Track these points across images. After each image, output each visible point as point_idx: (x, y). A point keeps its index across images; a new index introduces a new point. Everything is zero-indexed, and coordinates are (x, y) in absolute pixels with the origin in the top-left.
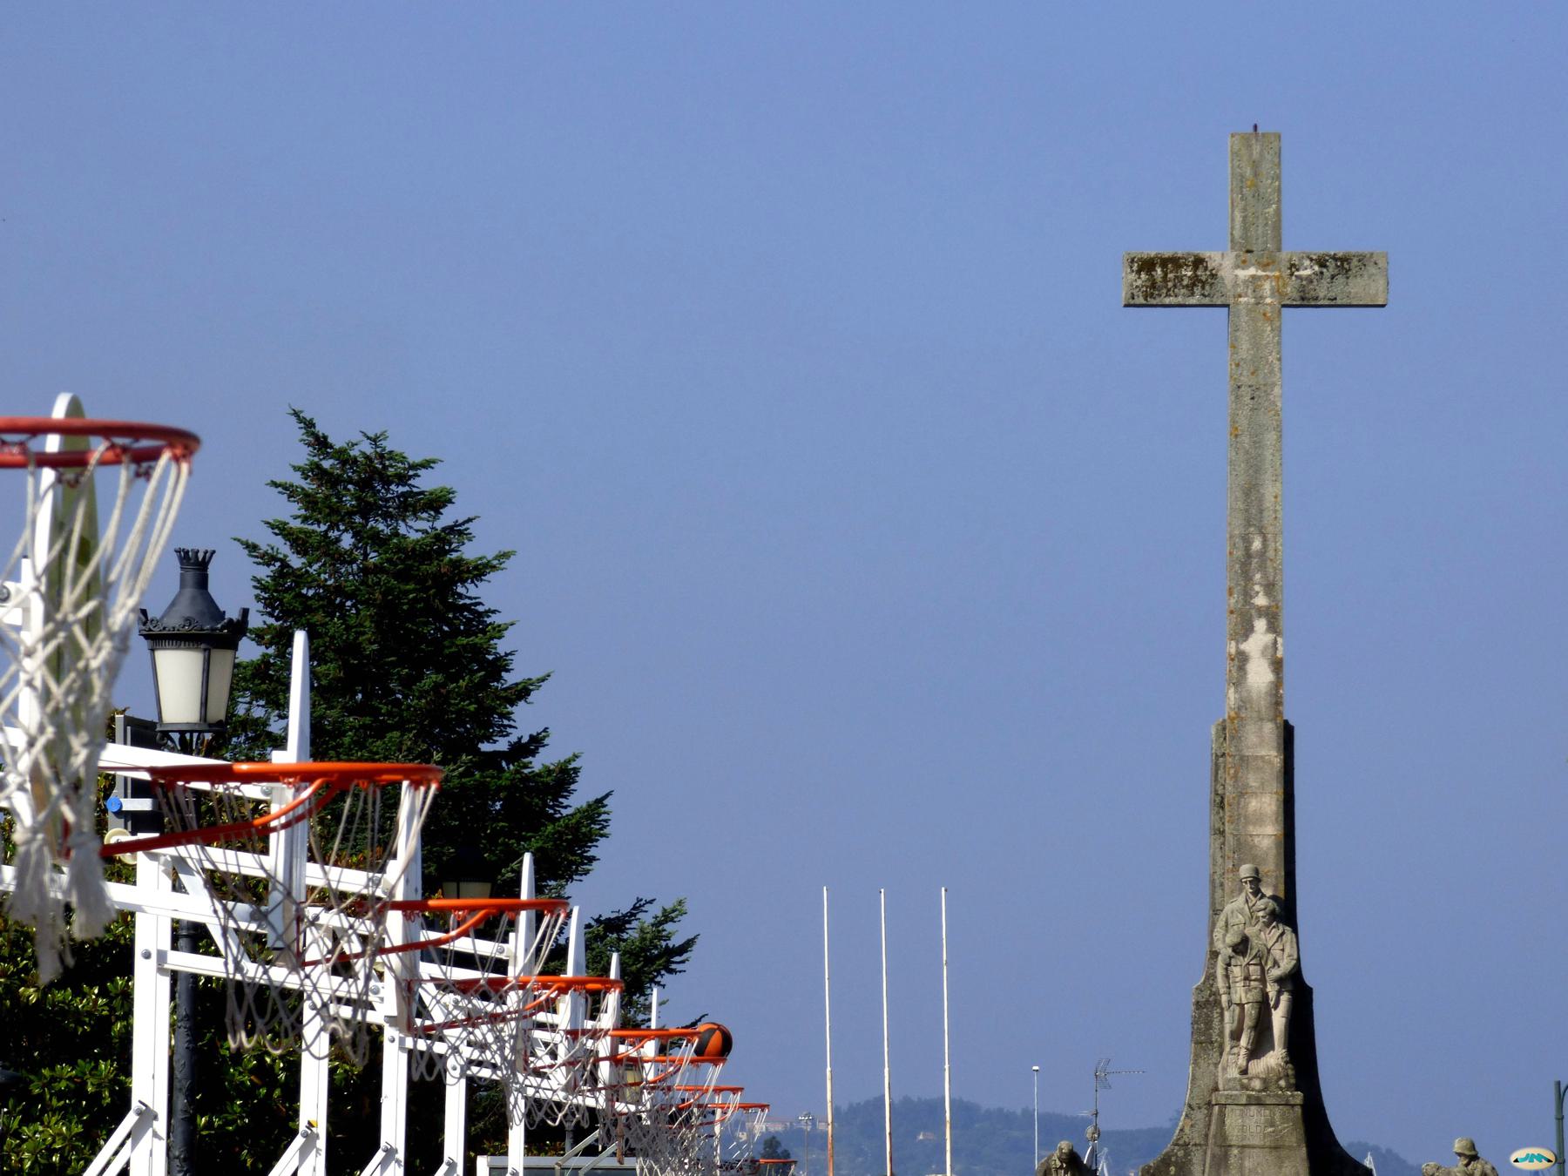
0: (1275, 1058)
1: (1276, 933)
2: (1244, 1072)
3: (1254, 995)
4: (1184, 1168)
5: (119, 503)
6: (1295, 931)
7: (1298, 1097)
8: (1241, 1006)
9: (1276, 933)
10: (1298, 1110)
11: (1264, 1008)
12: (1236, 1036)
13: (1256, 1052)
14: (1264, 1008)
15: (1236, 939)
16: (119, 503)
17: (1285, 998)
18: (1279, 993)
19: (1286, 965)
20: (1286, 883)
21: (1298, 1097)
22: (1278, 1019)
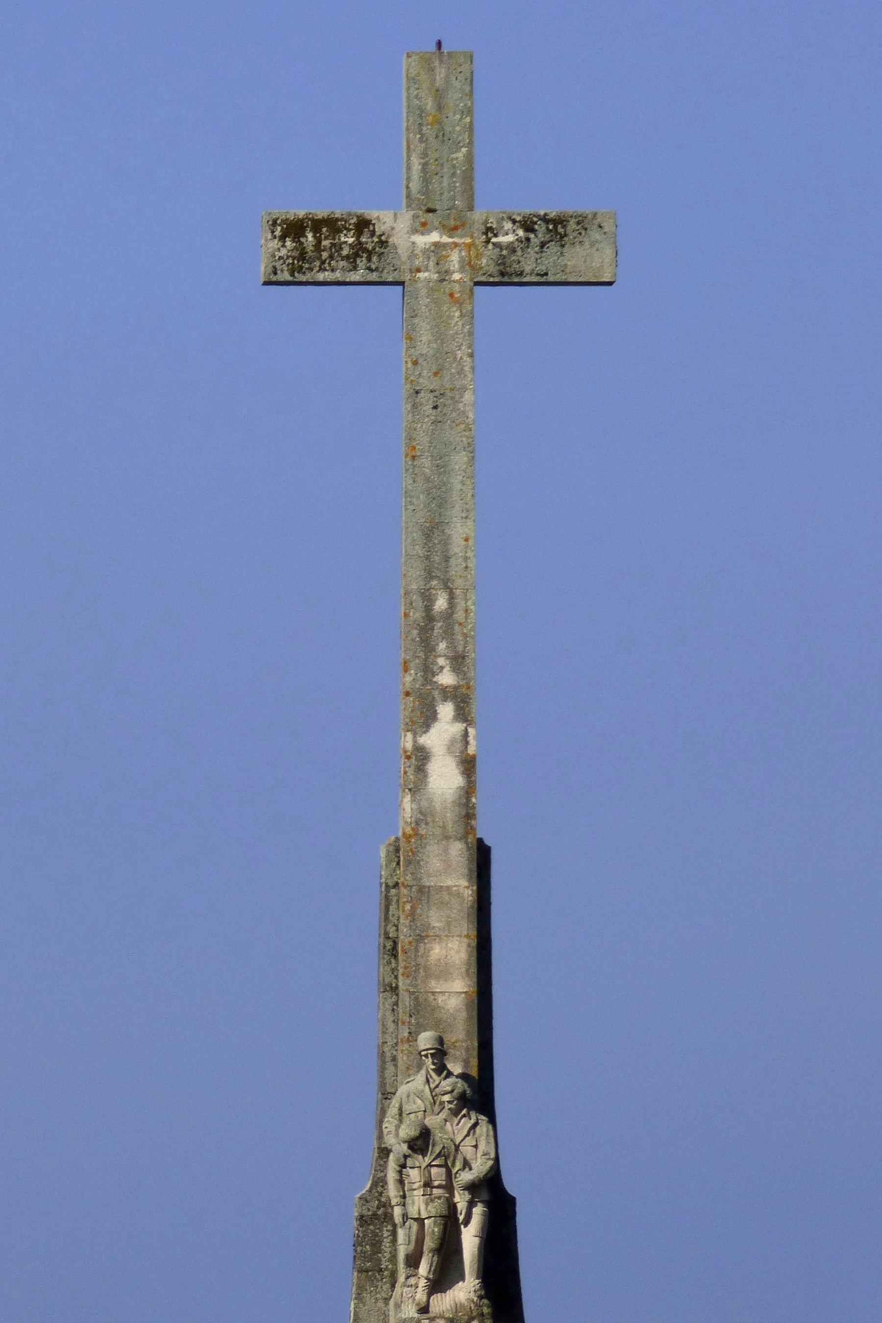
0: (465, 1290)
3: (437, 1207)
6: (492, 1121)
8: (420, 1221)
11: (451, 1224)
12: (413, 1261)
13: (441, 1281)
14: (451, 1224)
15: (413, 1132)
17: (478, 1210)
18: (471, 1204)
19: (480, 1167)
22: (470, 1239)
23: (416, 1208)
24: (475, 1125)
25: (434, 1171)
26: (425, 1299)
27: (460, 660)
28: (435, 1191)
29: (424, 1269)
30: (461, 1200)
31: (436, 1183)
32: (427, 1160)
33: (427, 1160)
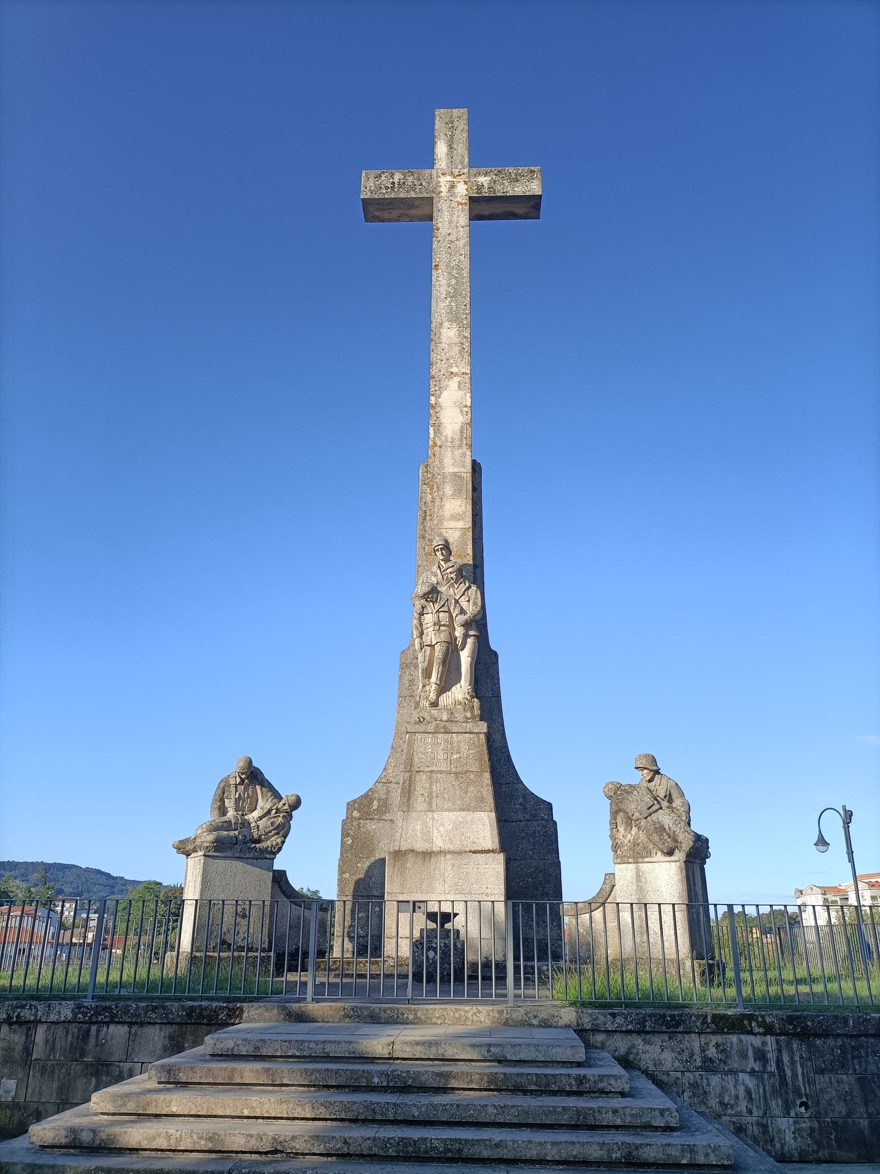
0: (461, 691)
1: (463, 587)
2: (435, 704)
3: (443, 636)
4: (305, 1173)
5: (450, 336)
6: (481, 588)
7: (483, 727)
8: (432, 646)
9: (463, 587)
10: (482, 736)
11: (452, 651)
12: (427, 674)
13: (444, 687)
14: (452, 651)
15: (426, 589)
16: (450, 336)
17: (470, 641)
18: (466, 636)
19: (471, 609)
20: (473, 477)
21: (483, 727)
22: (465, 657)
23: (429, 638)
24: (469, 588)
25: (441, 615)
26: (434, 698)
27: (638, 849)
28: (442, 628)
29: (434, 679)
30: (459, 632)
31: (443, 623)
32: (437, 606)
33: (437, 606)
